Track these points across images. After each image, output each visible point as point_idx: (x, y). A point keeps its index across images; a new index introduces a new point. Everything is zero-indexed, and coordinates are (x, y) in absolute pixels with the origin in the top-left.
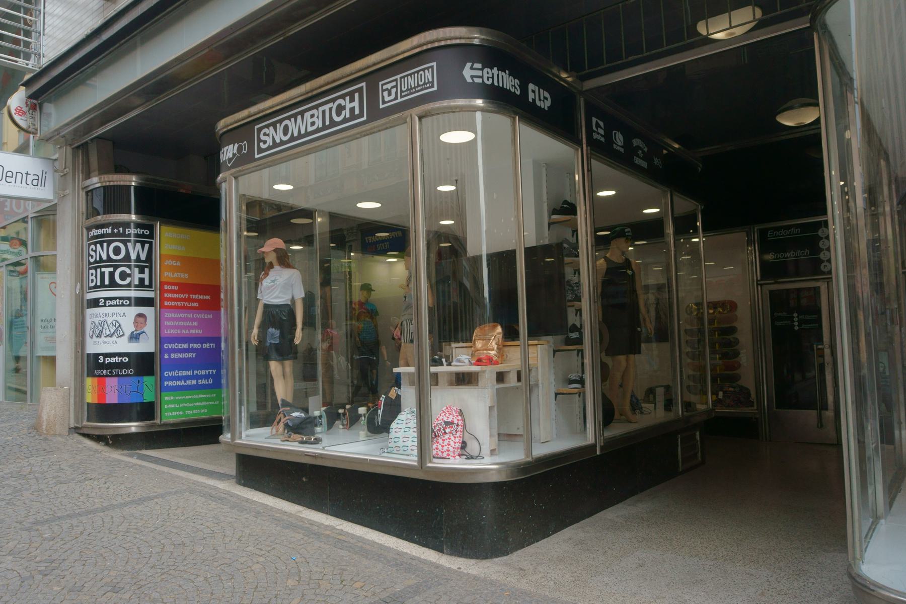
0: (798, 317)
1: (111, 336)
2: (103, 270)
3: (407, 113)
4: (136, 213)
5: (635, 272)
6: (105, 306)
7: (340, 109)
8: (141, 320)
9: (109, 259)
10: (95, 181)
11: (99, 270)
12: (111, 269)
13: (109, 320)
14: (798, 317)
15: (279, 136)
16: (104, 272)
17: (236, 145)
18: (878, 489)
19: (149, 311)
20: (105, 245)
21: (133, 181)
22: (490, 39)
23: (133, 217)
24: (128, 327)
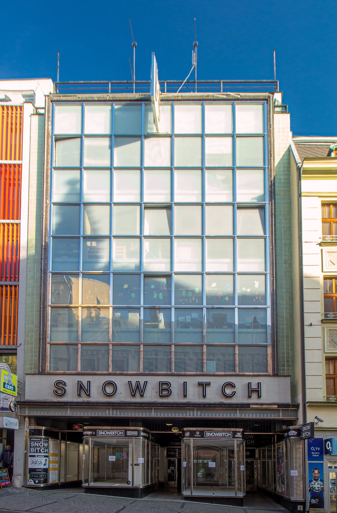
0: (178, 451)
1: (39, 464)
2: (37, 448)
3: (132, 437)
4: (44, 435)
5: (65, 382)
6: (37, 457)
7: (226, 435)
8: (46, 460)
9: (39, 446)
10: (33, 427)
11: (35, 448)
12: (40, 449)
13: (39, 460)
14: (178, 451)
15: (211, 435)
16: (37, 449)
17: (91, 432)
18: (184, 490)
19: (47, 458)
20: (38, 443)
21: (44, 428)
22: (23, 254)
23: (43, 437)
24: (44, 462)
